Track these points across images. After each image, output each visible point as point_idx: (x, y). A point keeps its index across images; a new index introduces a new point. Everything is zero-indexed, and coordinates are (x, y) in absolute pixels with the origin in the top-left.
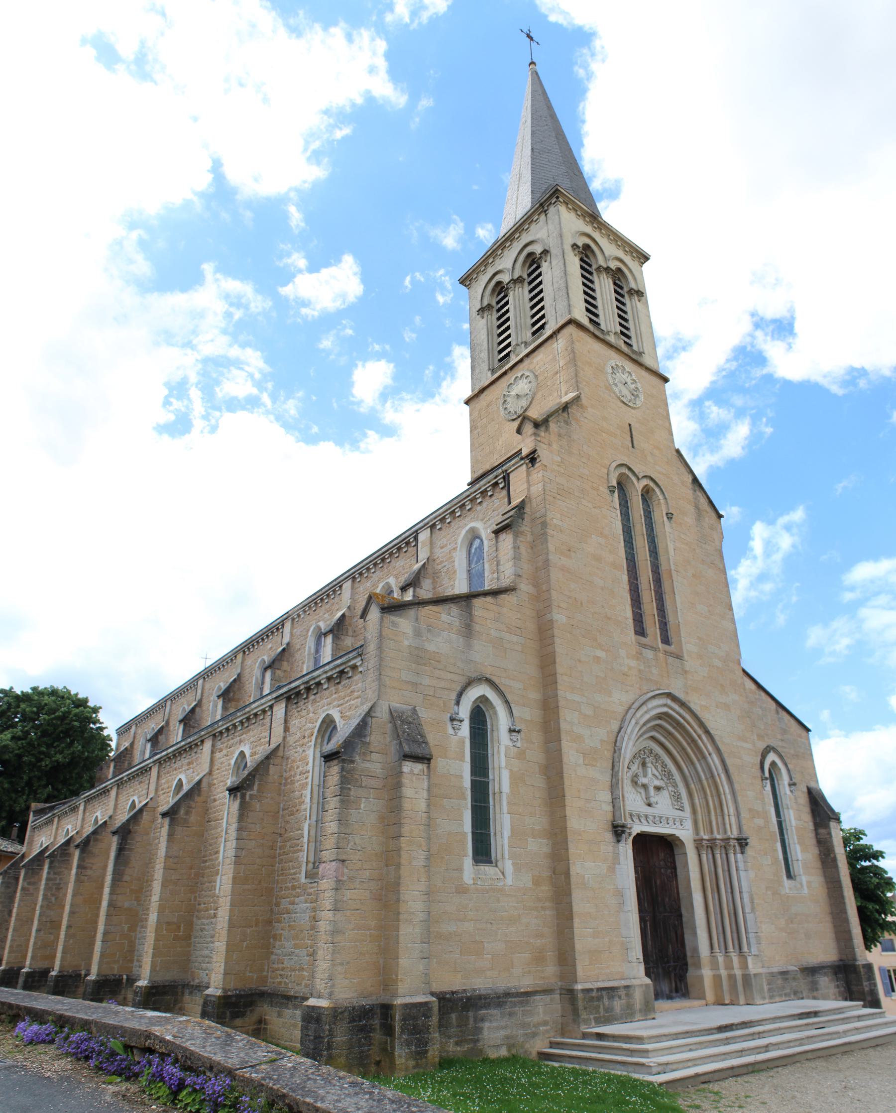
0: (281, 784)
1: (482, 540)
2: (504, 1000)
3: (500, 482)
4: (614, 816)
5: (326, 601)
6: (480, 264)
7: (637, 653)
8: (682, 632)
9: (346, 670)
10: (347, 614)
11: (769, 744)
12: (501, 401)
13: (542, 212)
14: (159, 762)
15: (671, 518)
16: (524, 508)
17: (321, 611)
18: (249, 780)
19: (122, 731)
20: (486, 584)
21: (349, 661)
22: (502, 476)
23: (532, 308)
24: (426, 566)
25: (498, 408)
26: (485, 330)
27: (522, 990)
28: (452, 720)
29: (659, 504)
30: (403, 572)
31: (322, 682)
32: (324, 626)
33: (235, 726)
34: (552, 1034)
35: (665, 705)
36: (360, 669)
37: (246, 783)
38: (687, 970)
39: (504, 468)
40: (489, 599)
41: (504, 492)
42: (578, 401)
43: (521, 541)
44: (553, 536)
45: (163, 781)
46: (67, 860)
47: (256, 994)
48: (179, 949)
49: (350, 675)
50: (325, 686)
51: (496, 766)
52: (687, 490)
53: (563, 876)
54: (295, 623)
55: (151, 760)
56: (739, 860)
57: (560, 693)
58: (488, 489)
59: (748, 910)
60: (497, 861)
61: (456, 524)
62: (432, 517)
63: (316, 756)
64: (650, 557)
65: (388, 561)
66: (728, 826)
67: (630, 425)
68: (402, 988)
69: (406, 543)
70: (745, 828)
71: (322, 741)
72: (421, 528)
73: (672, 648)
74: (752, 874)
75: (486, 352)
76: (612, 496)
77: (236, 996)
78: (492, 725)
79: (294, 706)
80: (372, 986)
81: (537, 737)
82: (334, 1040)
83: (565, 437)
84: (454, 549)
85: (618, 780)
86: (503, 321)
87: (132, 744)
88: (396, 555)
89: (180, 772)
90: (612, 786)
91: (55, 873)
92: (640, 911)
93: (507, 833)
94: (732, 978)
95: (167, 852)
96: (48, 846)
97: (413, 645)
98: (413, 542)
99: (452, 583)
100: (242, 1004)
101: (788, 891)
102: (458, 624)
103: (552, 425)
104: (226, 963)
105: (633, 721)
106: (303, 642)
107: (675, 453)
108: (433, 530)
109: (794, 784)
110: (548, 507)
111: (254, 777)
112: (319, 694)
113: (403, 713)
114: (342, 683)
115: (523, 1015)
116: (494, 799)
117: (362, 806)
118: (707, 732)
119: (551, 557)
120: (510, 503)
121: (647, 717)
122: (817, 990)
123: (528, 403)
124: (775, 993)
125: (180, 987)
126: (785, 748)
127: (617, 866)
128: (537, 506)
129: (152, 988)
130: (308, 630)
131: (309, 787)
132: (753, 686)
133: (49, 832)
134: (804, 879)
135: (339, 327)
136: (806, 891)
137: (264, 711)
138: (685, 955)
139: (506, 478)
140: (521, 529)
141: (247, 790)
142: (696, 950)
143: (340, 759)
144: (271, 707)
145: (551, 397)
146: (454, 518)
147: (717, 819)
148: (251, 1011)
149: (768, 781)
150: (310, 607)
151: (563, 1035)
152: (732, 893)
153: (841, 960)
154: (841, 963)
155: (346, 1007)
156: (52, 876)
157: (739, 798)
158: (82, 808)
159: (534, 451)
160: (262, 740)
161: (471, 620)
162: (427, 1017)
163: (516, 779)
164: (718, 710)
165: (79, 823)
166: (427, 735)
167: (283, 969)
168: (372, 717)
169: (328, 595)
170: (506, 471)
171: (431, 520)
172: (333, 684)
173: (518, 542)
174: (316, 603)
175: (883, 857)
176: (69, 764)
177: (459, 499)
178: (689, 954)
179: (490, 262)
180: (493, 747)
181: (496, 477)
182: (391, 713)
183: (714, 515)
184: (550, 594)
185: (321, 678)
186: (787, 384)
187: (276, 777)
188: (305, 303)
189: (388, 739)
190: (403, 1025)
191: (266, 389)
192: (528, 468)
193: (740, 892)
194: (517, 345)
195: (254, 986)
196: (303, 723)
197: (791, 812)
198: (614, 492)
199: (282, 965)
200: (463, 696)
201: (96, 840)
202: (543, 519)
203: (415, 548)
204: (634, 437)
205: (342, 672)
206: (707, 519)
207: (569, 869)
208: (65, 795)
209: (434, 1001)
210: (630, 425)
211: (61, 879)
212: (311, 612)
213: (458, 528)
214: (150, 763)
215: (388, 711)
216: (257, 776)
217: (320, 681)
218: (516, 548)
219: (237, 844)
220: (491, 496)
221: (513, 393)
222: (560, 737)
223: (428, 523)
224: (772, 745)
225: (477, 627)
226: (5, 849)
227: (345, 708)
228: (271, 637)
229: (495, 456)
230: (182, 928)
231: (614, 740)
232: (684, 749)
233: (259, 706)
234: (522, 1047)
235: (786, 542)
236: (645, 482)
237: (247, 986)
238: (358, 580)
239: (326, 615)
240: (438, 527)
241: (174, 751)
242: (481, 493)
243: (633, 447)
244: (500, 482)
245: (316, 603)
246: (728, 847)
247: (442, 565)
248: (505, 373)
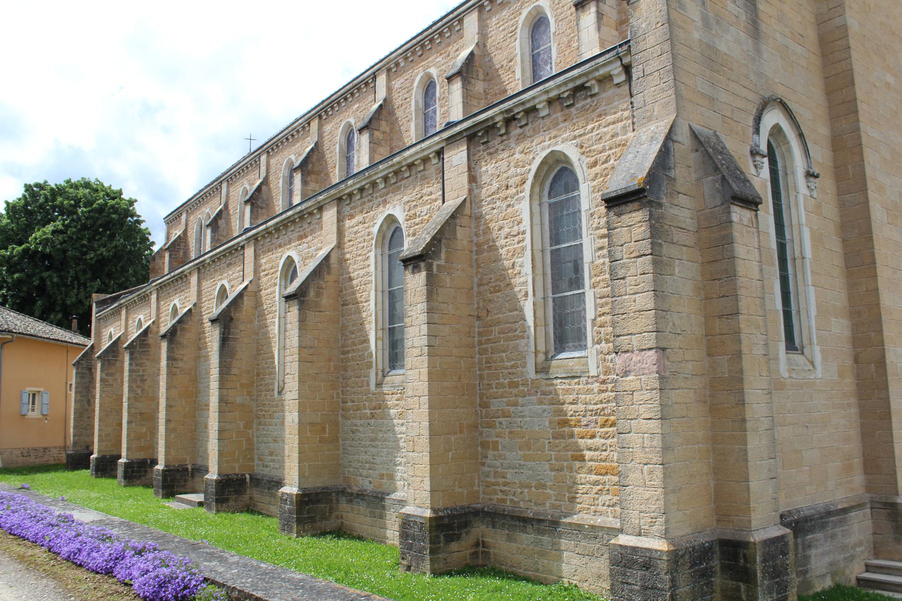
0: (472, 252)
2: (827, 520)
5: (438, 41)
9: (587, 85)
10: (475, 53)
14: (255, 238)
18: (434, 245)
19: (172, 219)
21: (597, 69)
27: (840, 507)
33: (374, 184)
34: (866, 555)
37: (431, 250)
45: (263, 261)
46: (148, 351)
47: (470, 513)
48: (327, 453)
51: (794, 222)
53: (873, 366)
54: (391, 74)
55: (244, 237)
60: (803, 347)
63: (534, 211)
68: (756, 518)
71: (541, 191)
77: (449, 516)
78: (785, 167)
79: (482, 147)
80: (705, 517)
82: (677, 592)
87: (185, 232)
89: (288, 249)
91: (137, 365)
93: (813, 311)
95: (300, 341)
96: (119, 337)
100: (456, 525)
104: (432, 478)
111: (440, 241)
112: (530, 126)
114: (578, 105)
115: (843, 536)
116: (795, 266)
117: (677, 271)
125: (334, 494)
129: (304, 495)
131: (528, 253)
133: (118, 323)
137: (426, 160)
141: (434, 259)
143: (644, 201)
144: (440, 153)
148: (467, 533)
150: (414, 53)
151: (877, 555)
155: (687, 548)
156: (134, 367)
158: (154, 297)
160: (425, 198)
161: (757, 15)
162: (784, 553)
163: (817, 239)
165: (154, 312)
167: (505, 484)
176: (115, 256)
185: (537, 101)
187: (465, 242)
190: (764, 567)
195: (465, 504)
196: (504, 168)
199: (503, 480)
201: (183, 329)
207: (884, 357)
208: (113, 289)
209: (789, 533)
211: (143, 371)
212: (416, 58)
214: (243, 241)
216: (444, 241)
219: (428, 329)
226: (70, 340)
228: (357, 95)
230: (327, 430)
233: (417, 153)
234: (844, 574)
237: (458, 504)
238: (488, 9)
241: (277, 223)
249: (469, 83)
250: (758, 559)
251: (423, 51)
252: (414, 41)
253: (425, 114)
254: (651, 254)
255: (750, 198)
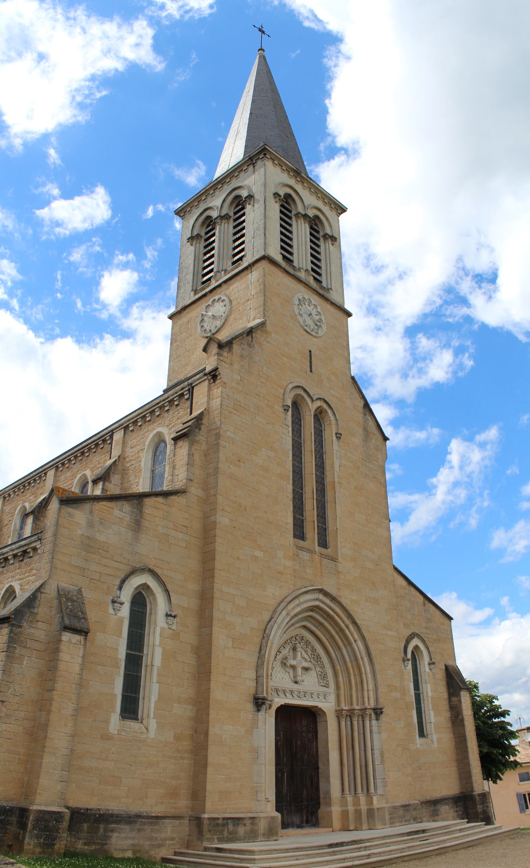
1: (166, 445)
3: (185, 393)
4: (256, 691)
5: (33, 485)
6: (226, 176)
7: (294, 554)
8: (338, 538)
9: (28, 551)
11: (414, 631)
12: (200, 319)
13: (251, 164)
15: (340, 438)
16: (202, 420)
17: (28, 494)
20: (165, 485)
21: (31, 543)
22: (187, 388)
23: (235, 234)
24: (117, 463)
25: (197, 325)
26: (193, 255)
28: (114, 602)
29: (330, 424)
30: (98, 466)
31: (9, 558)
32: (29, 507)
35: (317, 599)
36: (39, 551)
38: (319, 807)
39: (190, 381)
40: (160, 499)
41: (188, 403)
42: (263, 327)
43: (195, 449)
44: (225, 447)
49: (31, 555)
50: (11, 562)
51: (151, 643)
52: (359, 415)
54: (6, 501)
56: (373, 725)
57: (216, 586)
58: (175, 399)
59: (377, 762)
60: (142, 719)
61: (145, 428)
62: (126, 419)
64: (316, 471)
65: (87, 454)
66: (366, 699)
67: (310, 351)
69: (103, 440)
70: (381, 700)
72: (116, 428)
73: (329, 551)
74: (384, 735)
75: (192, 275)
76: (286, 414)
78: (151, 609)
81: (192, 622)
83: (247, 358)
84: (142, 450)
85: (264, 662)
86: (209, 248)
88: (94, 450)
90: (257, 666)
92: (277, 764)
94: (358, 812)
97: (85, 534)
98: (108, 440)
99: (137, 480)
101: (419, 746)
102: (128, 519)
103: (236, 347)
105: (284, 613)
106: (10, 519)
107: (350, 380)
108: (127, 431)
109: (434, 663)
110: (223, 420)
113: (69, 592)
114: (25, 561)
117: (25, 662)
118: (354, 623)
119: (220, 465)
120: (191, 413)
121: (298, 609)
122: (437, 815)
123: (222, 324)
124: (396, 821)
126: (429, 634)
127: (255, 730)
128: (214, 418)
130: (16, 509)
132: (404, 583)
134: (435, 737)
135: (89, 244)
136: (436, 745)
138: (318, 797)
139: (191, 391)
140: (197, 439)
142: (328, 793)
145: (241, 321)
146: (145, 422)
147: (357, 693)
149: (410, 662)
150: (19, 489)
152: (365, 750)
153: (462, 793)
154: (462, 795)
157: (379, 677)
159: (216, 369)
161: (141, 517)
164: (367, 604)
166: (88, 612)
168: (41, 593)
169: (35, 480)
170: (191, 384)
171: (125, 422)
172: (18, 561)
173: (193, 449)
174: (24, 486)
175: (509, 715)
177: (150, 405)
178: (322, 796)
179: (227, 181)
180: (150, 628)
181: (183, 389)
182: (58, 591)
183: (380, 437)
184: (216, 498)
185: (9, 554)
186: (484, 327)
188: (58, 224)
189: (54, 612)
191: (16, 296)
192: (210, 384)
193: (372, 750)
194: (218, 272)
197: (429, 686)
198: (288, 410)
200: (126, 583)
202: (217, 431)
203: (110, 445)
204: (313, 362)
205: (25, 552)
206: (373, 441)
210: (310, 351)
212: (20, 494)
213: (148, 431)
215: (56, 589)
217: (7, 557)
218: (190, 455)
220: (177, 405)
221: (210, 314)
222: (212, 623)
223: (122, 425)
224: (417, 632)
225: (145, 523)
227: (24, 582)
229: (189, 368)
231: (263, 628)
232: (332, 637)
235: (476, 456)
236: (318, 403)
238: (61, 469)
239: (31, 498)
240: (131, 429)
242: (169, 401)
243: (311, 371)
244: (185, 393)
245: (24, 486)
246: (364, 716)
247: (131, 464)
248: (205, 295)
249: (39, 519)
250: (31, 818)
251: (24, 490)
252: (20, 482)
253: (19, 534)
254: (6, 652)
255: (73, 627)
